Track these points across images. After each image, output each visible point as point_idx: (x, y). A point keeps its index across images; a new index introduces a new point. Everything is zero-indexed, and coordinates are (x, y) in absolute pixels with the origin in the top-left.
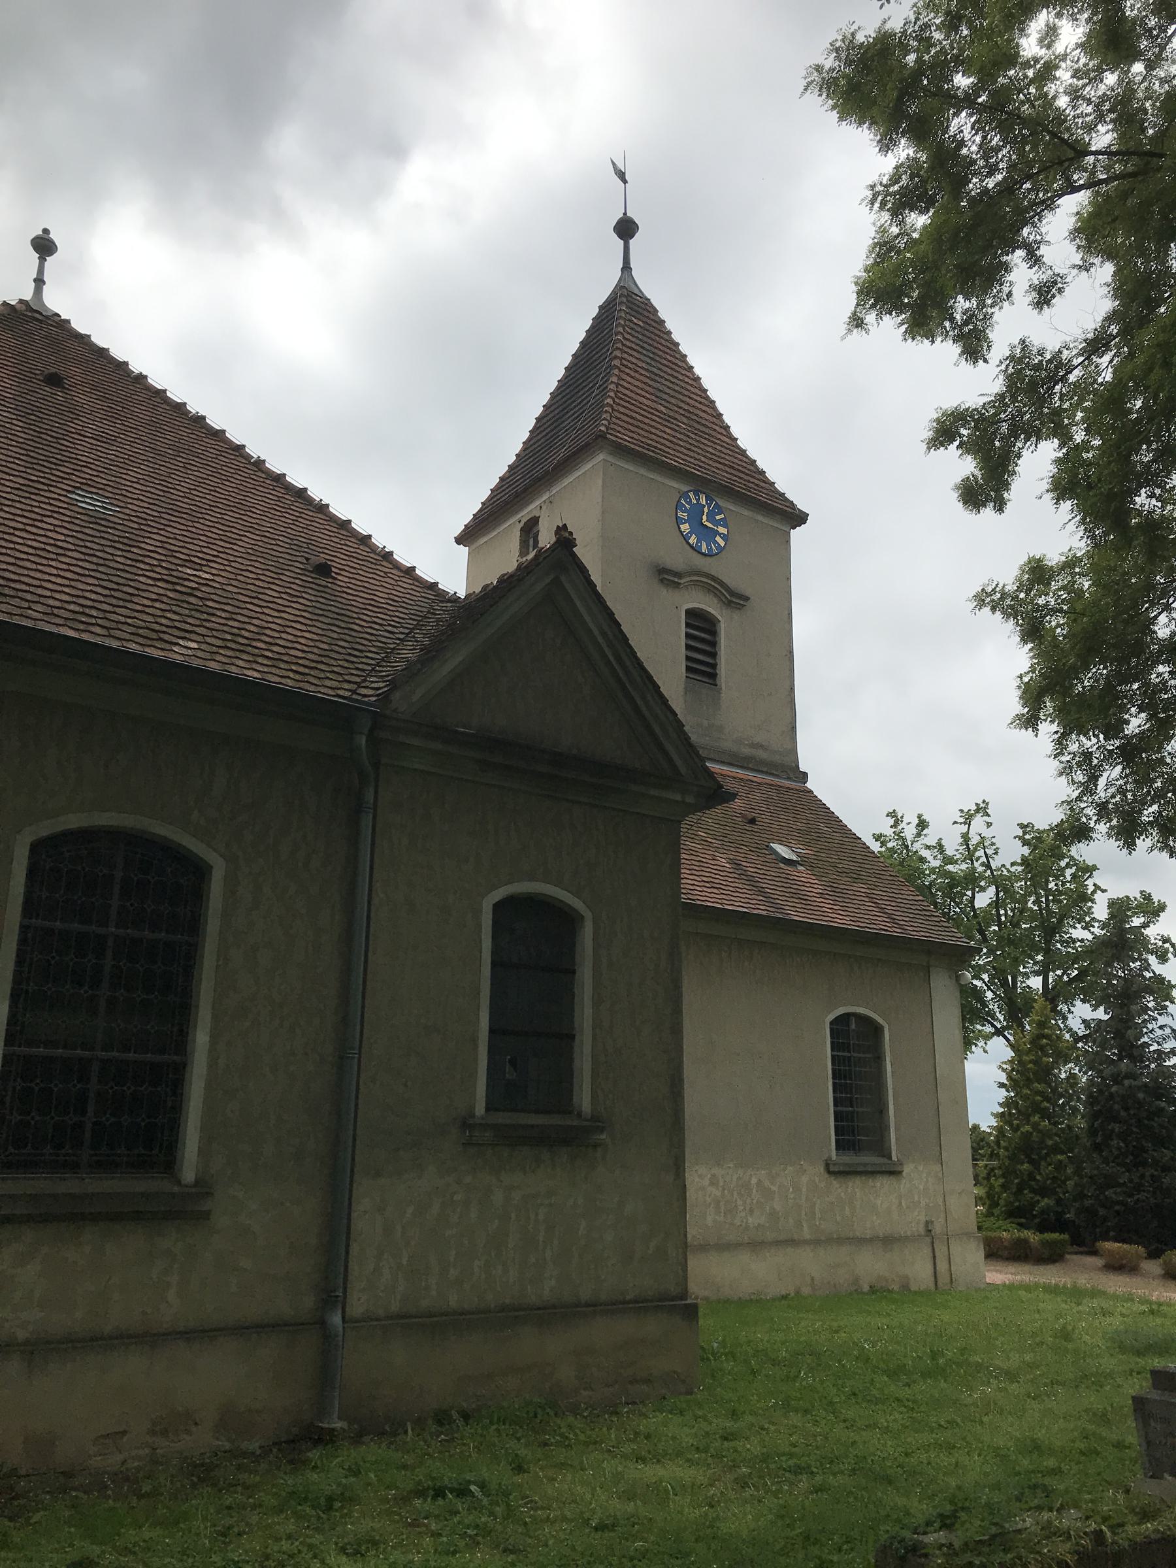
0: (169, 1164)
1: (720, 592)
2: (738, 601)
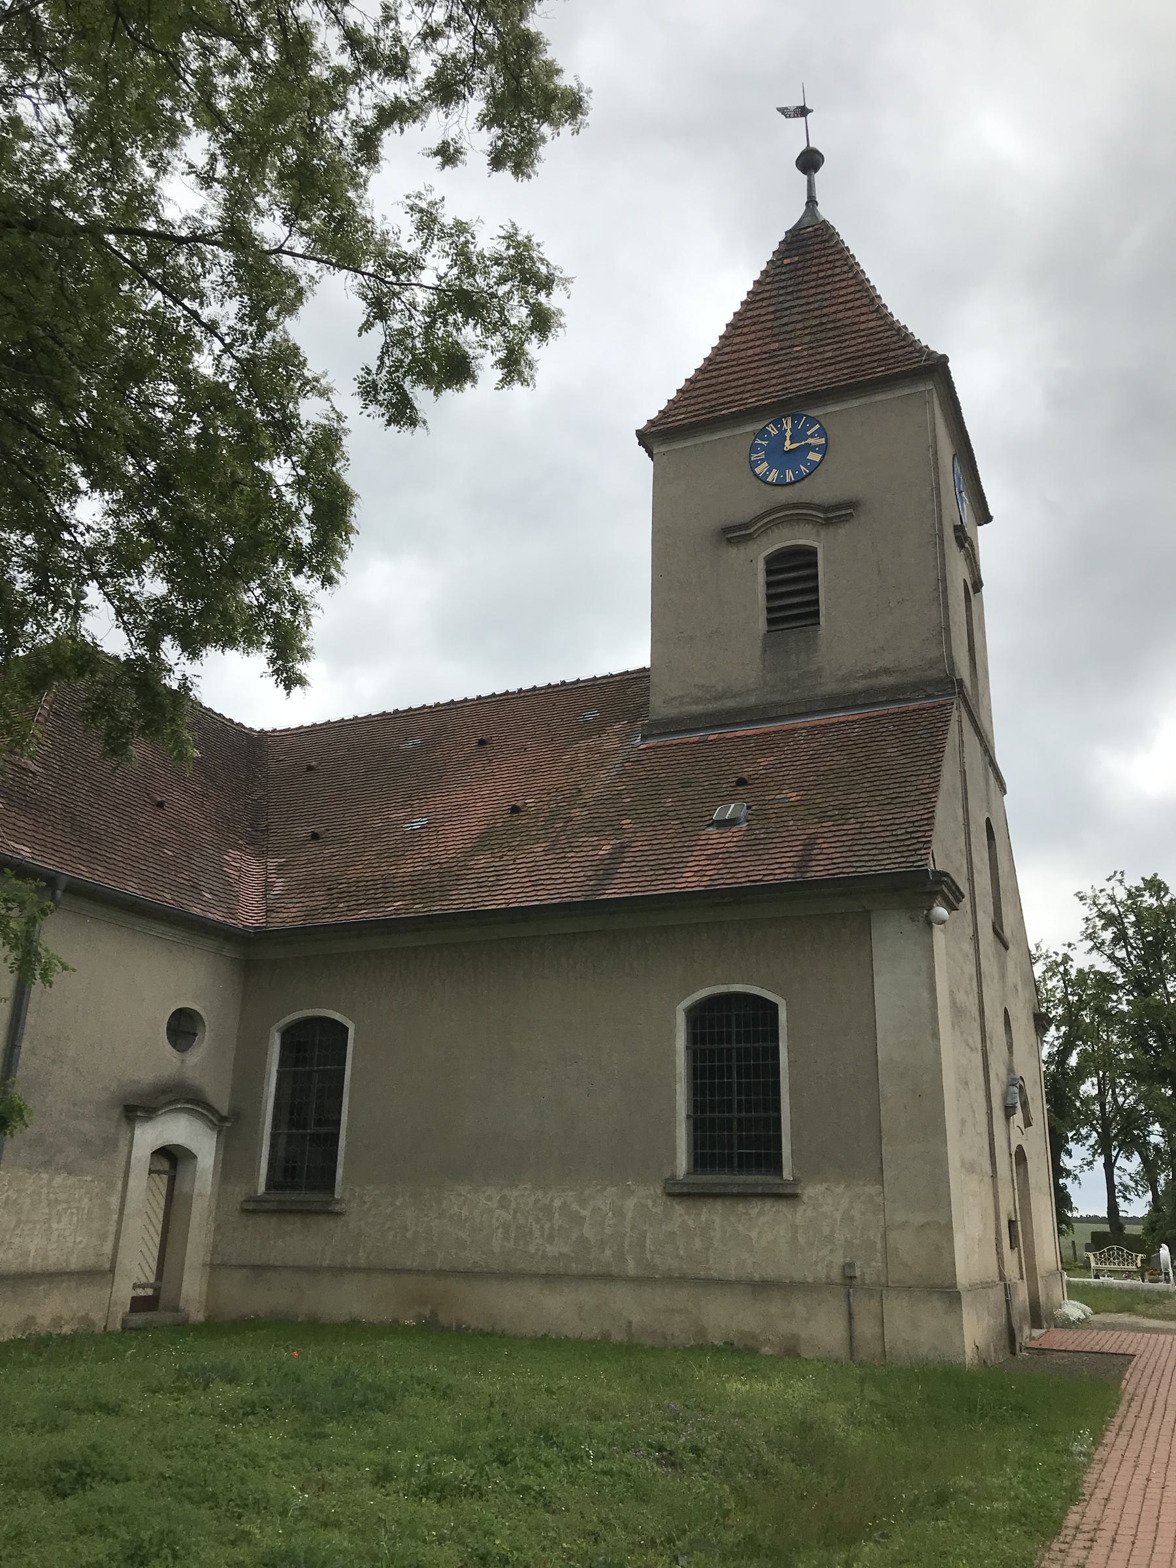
0: (776, 1165)
1: (810, 515)
2: (838, 513)
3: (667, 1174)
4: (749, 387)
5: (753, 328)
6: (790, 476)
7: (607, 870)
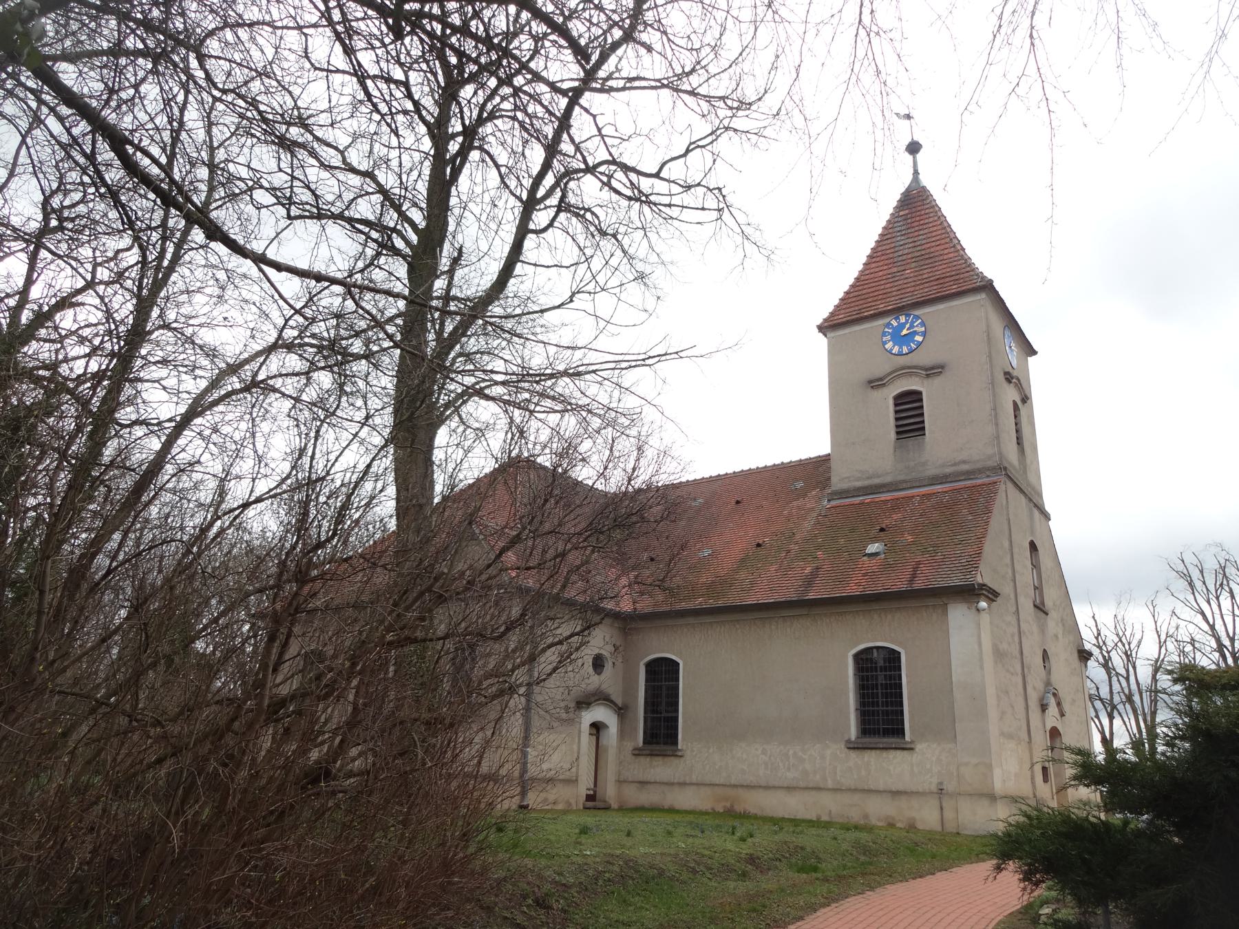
3: (846, 738)
4: (880, 297)
5: (883, 258)
6: (905, 350)
7: (809, 582)
